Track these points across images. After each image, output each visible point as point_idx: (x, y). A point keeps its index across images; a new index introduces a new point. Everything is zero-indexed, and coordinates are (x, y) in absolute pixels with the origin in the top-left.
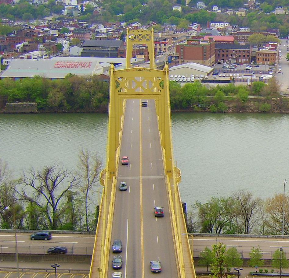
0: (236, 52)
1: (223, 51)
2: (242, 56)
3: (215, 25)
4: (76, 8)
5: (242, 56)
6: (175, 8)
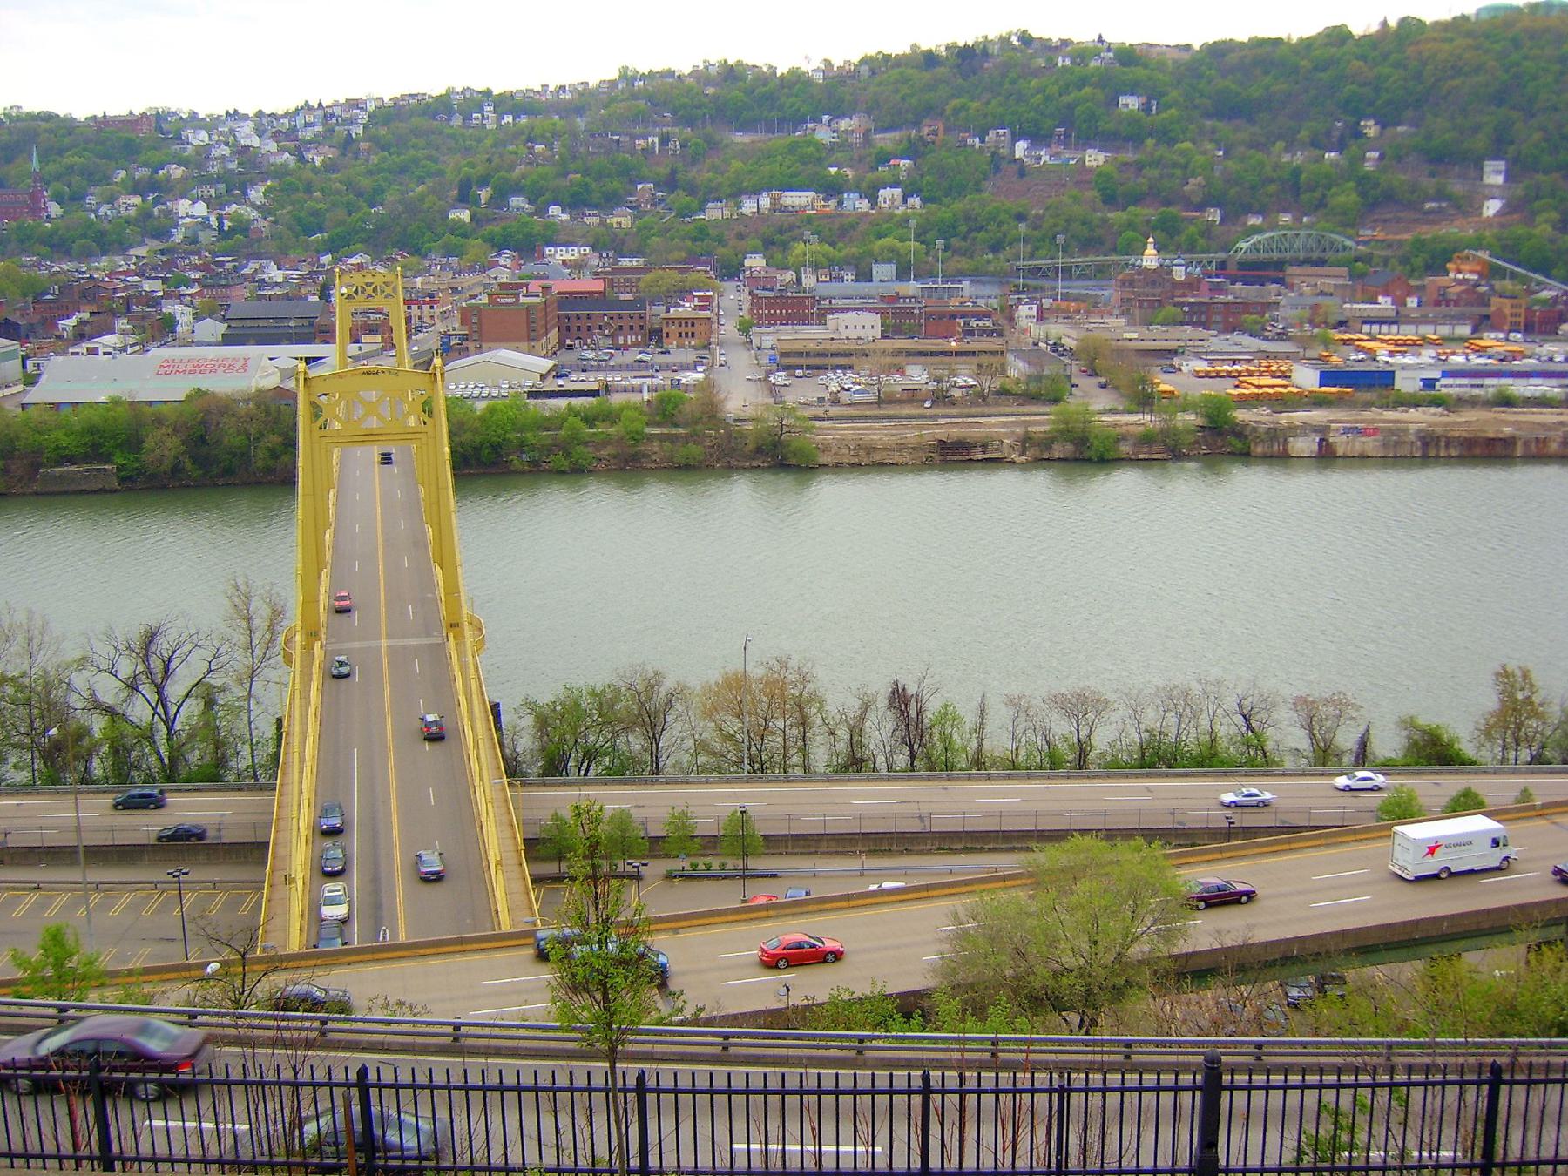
1: (578, 317)
2: (626, 328)
4: (205, 223)
5: (626, 328)
6: (454, 215)
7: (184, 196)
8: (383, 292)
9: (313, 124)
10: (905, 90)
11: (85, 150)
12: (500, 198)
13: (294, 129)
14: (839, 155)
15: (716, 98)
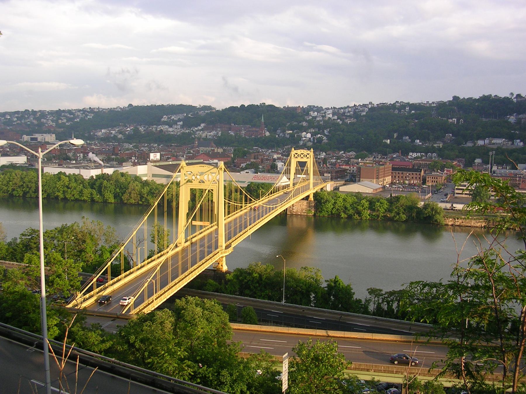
0: (410, 174)
3: (413, 154)
4: (310, 140)
8: (298, 155)
12: (400, 137)
13: (344, 113)
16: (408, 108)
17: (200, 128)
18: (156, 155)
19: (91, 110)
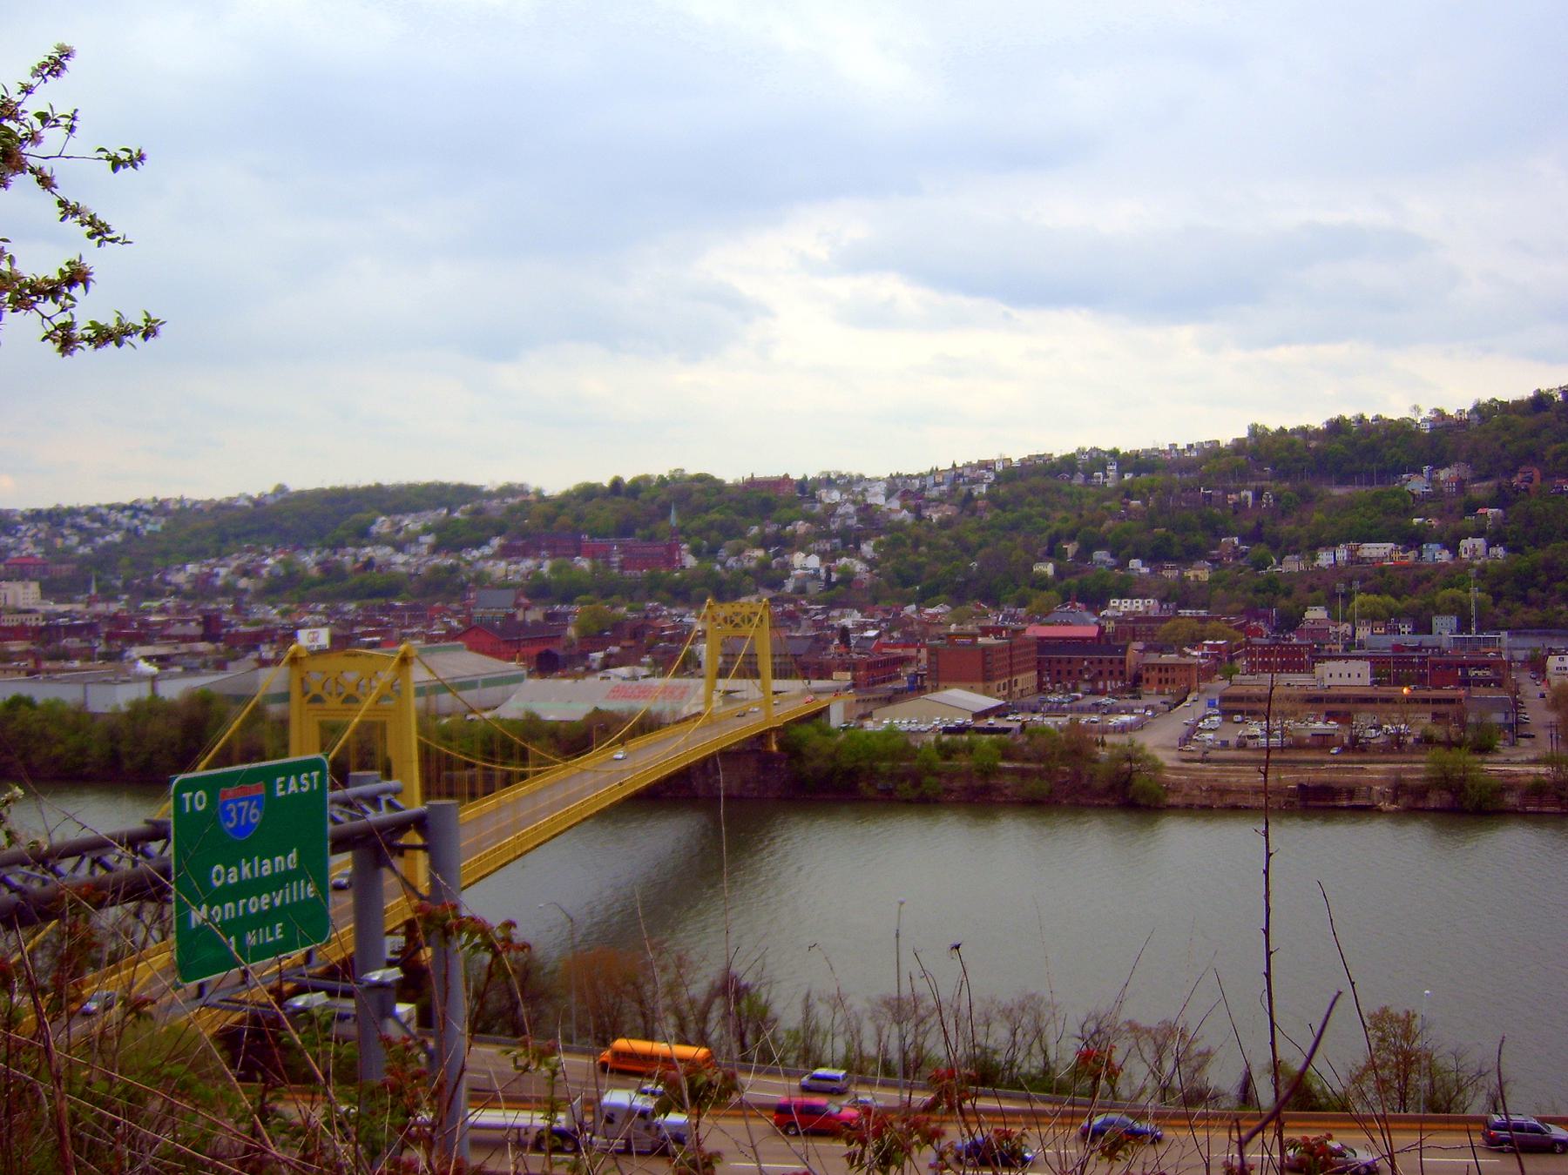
0: (1091, 663)
1: (1059, 661)
2: (1106, 674)
3: (1120, 603)
4: (815, 576)
5: (1106, 674)
6: (1038, 568)
7: (802, 549)
9: (942, 484)
10: (1505, 437)
11: (728, 507)
12: (1085, 553)
14: (1429, 506)
15: (1317, 450)
16: (1115, 467)
17: (487, 550)
18: (316, 635)
19: (161, 508)
